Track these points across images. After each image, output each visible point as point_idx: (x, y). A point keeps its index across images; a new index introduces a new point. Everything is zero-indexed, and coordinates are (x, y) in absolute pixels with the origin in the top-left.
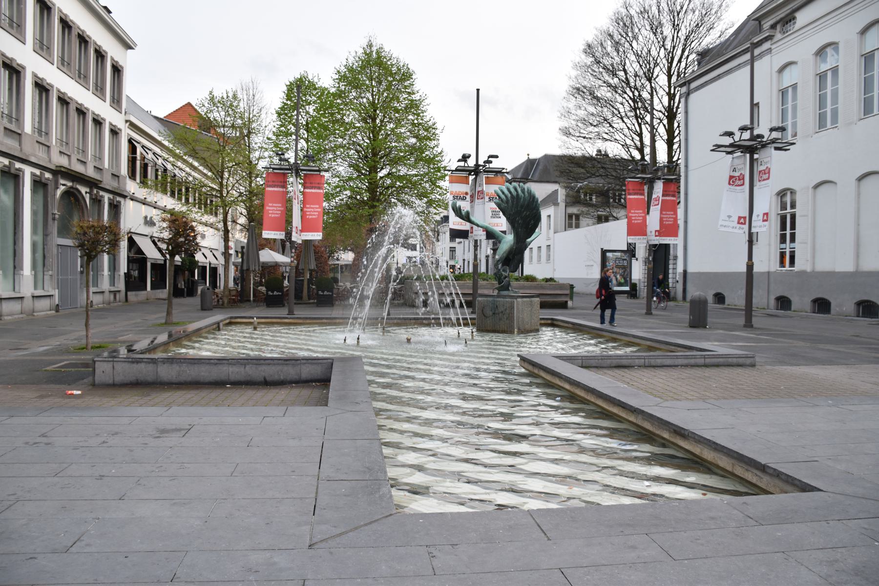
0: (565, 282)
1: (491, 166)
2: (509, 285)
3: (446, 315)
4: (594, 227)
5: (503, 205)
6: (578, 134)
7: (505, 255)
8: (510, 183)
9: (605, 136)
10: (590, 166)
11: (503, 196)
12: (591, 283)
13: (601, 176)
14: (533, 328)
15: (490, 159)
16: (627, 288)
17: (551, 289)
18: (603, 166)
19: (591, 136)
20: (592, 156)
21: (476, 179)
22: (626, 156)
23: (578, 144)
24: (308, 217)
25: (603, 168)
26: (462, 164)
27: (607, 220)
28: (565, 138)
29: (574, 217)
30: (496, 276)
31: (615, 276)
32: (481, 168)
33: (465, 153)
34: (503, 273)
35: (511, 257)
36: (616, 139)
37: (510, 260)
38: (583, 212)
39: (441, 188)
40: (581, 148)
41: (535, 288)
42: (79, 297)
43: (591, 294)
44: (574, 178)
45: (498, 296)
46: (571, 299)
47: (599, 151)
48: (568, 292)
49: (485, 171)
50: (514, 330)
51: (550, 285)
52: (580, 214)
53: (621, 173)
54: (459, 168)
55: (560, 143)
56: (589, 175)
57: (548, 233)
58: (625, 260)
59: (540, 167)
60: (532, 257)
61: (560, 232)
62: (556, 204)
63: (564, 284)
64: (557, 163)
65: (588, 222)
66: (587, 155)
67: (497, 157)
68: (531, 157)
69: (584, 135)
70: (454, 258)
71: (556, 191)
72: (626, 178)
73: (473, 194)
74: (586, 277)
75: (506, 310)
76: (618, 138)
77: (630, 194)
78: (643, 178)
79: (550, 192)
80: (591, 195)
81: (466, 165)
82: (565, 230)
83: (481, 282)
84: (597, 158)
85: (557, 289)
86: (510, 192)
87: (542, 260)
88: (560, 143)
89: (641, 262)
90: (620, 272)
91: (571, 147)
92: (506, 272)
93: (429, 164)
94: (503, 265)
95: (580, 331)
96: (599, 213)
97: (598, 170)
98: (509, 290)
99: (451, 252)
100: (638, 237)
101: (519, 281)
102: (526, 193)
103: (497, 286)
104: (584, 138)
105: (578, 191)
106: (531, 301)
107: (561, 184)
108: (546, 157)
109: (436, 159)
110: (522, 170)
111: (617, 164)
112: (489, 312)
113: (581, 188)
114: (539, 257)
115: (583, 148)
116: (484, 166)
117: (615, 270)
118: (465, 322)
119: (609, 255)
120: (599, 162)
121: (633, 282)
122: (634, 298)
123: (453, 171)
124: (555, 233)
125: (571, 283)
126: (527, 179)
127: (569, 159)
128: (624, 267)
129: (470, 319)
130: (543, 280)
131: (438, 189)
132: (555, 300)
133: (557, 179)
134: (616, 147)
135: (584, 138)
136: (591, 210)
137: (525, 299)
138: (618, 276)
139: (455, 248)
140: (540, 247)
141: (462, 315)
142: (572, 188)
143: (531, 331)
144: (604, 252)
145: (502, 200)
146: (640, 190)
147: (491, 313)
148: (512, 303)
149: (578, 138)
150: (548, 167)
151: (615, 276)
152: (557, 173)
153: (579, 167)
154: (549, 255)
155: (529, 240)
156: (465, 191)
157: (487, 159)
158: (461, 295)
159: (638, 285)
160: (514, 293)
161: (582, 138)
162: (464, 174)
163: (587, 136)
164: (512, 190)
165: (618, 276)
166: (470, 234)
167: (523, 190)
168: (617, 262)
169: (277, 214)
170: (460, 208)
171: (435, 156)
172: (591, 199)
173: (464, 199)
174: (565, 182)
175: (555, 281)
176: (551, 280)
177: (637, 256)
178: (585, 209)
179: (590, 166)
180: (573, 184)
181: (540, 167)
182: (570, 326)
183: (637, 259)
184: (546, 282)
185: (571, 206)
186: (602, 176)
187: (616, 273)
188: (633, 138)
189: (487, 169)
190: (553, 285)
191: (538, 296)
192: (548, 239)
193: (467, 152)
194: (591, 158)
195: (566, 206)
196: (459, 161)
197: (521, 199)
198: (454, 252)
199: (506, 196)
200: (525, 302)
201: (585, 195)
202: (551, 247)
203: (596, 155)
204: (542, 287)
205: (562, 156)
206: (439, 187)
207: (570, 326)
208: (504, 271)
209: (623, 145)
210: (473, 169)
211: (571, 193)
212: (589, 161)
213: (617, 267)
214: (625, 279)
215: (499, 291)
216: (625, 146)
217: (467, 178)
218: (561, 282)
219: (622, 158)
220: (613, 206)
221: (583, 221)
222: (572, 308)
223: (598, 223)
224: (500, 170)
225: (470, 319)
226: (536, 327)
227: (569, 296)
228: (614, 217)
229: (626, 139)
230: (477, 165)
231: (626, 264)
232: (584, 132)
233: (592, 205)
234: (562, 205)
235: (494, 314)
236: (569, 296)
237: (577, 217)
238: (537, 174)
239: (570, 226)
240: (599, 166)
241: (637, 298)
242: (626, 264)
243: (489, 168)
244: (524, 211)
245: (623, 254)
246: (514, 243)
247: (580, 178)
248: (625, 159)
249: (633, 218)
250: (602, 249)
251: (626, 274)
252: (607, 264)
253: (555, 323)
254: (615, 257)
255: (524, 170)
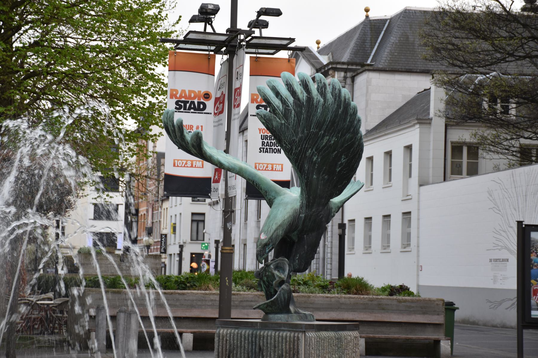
0: (434, 296)
1: (266, 33)
4: (510, 171)
5: (277, 122)
7: (281, 232)
8: (326, 74)
10: (506, 34)
11: (276, 102)
12: (504, 301)
15: (262, 18)
21: (230, 62)
26: (199, 27)
29: (465, 150)
30: (261, 279)
32: (242, 37)
33: (205, 2)
34: (276, 273)
35: (294, 236)
37: (294, 243)
38: (484, 138)
41: (365, 308)
43: (504, 327)
44: (465, 62)
45: (265, 326)
48: (440, 319)
49: (249, 45)
51: (399, 301)
52: (480, 144)
54: (191, 36)
56: (499, 55)
57: (406, 186)
59: (393, 39)
60: (370, 237)
61: (433, 184)
63: (430, 300)
64: (427, 29)
65: (496, 162)
66: (498, 10)
67: (277, 13)
68: (374, 15)
70: (200, 237)
71: (427, 91)
73: (223, 95)
74: (491, 285)
79: (413, 94)
80: (506, 100)
81: (209, 29)
82: (445, 180)
83: (235, 289)
84: (523, 15)
85: (415, 312)
86: (293, 92)
92: (283, 271)
94: (276, 256)
96: (523, 141)
97: (522, 46)
98: (288, 312)
99: (195, 225)
101: (329, 291)
102: (329, 96)
103: (263, 301)
105: (476, 93)
106: (339, 339)
107: (437, 76)
109: (147, 13)
110: (352, 44)
116: (248, 33)
120: (525, 26)
123: (178, 42)
124: (421, 185)
125: (447, 299)
126: (363, 65)
127: (455, 21)
130: (384, 289)
132: (410, 336)
133: (431, 66)
136: (504, 134)
137: (324, 334)
139: (203, 214)
142: (463, 87)
145: (274, 111)
150: (411, 39)
152: (428, 52)
153: (478, 37)
154: (409, 234)
155: (336, 200)
156: (203, 90)
157: (254, 17)
160: (301, 319)
162: (202, 50)
170: (181, 126)
172: (506, 111)
173: (200, 108)
174: (445, 72)
175: (411, 294)
176: (403, 289)
178: (489, 133)
179: (506, 34)
180: (463, 78)
181: (393, 39)
184: (391, 294)
185: (457, 124)
189: (254, 41)
190: (405, 301)
191: (356, 325)
192: (407, 198)
196: (193, 20)
197: (303, 103)
198: (201, 225)
199: (284, 102)
200: (324, 339)
201: (493, 100)
202: (414, 216)
204: (381, 307)
205: (440, 13)
206: (152, 77)
208: (277, 268)
210: (223, 38)
211: (458, 96)
212: (502, 24)
215: (267, 313)
217: (210, 59)
218: (425, 295)
223: (521, 165)
224: (285, 42)
227: (443, 330)
230: (233, 31)
233: (507, 125)
234: (439, 124)
236: (443, 330)
238: (385, 54)
239: (457, 171)
243: (261, 37)
244: (324, 136)
246: (301, 207)
247: (478, 63)
248: (495, 14)
250: (520, 223)
255: (356, 45)
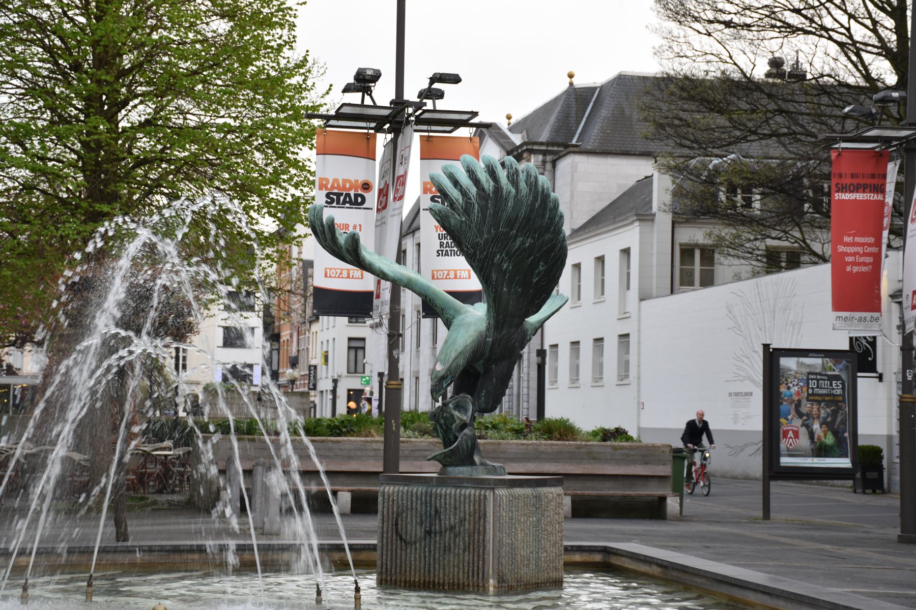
0: (658, 441)
1: (441, 105)
2: (473, 448)
3: (270, 534)
5: (456, 219)
6: (710, 15)
7: (462, 362)
8: (519, 158)
9: (794, 20)
11: (455, 193)
12: (746, 445)
13: (774, 134)
14: (543, 576)
15: (436, 86)
16: (844, 463)
17: (617, 462)
18: (784, 106)
19: (748, 21)
20: (750, 80)
21: (394, 142)
22: (853, 78)
23: (708, 44)
24: (849, 269)
25: (781, 111)
26: (355, 98)
27: (794, 262)
28: (673, 25)
29: (697, 254)
30: (437, 421)
31: (808, 427)
32: (410, 110)
35: (479, 367)
36: (823, 28)
38: (721, 238)
39: (303, 168)
40: (717, 56)
41: (572, 457)
42: (346, 488)
43: (747, 478)
45: (442, 481)
46: (678, 491)
47: (776, 63)
48: (665, 470)
49: (419, 121)
50: (485, 580)
51: (615, 448)
53: (838, 127)
54: (345, 110)
55: (658, 41)
56: (738, 133)
57: (623, 300)
58: (837, 378)
61: (657, 297)
62: (645, 217)
64: (647, 99)
65: (736, 269)
66: (736, 76)
67: (455, 79)
69: (727, 18)
70: (360, 369)
71: (649, 178)
72: (835, 141)
75: (462, 521)
76: (828, 22)
77: (843, 189)
78: (887, 141)
79: (631, 182)
80: (747, 190)
81: (368, 101)
82: (672, 292)
84: (768, 83)
86: (476, 181)
87: (605, 376)
88: (658, 41)
89: (894, 385)
90: (823, 414)
91: (689, 54)
93: (268, 96)
95: (687, 588)
96: (770, 242)
98: (473, 463)
99: (352, 353)
100: (857, 315)
101: (525, 437)
102: (523, 185)
103: (440, 450)
104: (728, 24)
105: (710, 181)
106: (538, 497)
107: (661, 160)
108: (623, 82)
109: (289, 81)
110: (552, 119)
111: (825, 100)
112: (414, 530)
113: (717, 171)
114: (598, 368)
115: (725, 56)
116: (418, 106)
117: (806, 407)
118: (247, 556)
119: (787, 363)
120: (770, 96)
121: (861, 442)
122: (874, 492)
123: (327, 118)
126: (566, 146)
127: (683, 89)
128: (832, 401)
129: (352, 547)
130: (595, 434)
131: (293, 171)
133: (653, 147)
134: (820, 53)
135: (728, 24)
136: (746, 233)
137: (518, 491)
138: (816, 426)
139: (363, 339)
140: (601, 340)
141: (349, 536)
142: (694, 173)
143: (538, 586)
144: (772, 356)
145: (452, 205)
146: (873, 176)
147: (420, 532)
148: (483, 501)
149: (711, 27)
150: (628, 112)
151: (808, 427)
152: (648, 128)
153: (712, 110)
154: (627, 363)
155: (533, 319)
156: (361, 178)
157: (426, 86)
158: (323, 477)
159: (885, 453)
161: (722, 27)
162: (360, 128)
163: (736, 19)
164: (483, 176)
165: (816, 426)
166: (375, 301)
167: (513, 177)
168: (812, 384)
169: (865, 264)
171: (290, 72)
172: (748, 203)
173: (357, 202)
174: (671, 154)
176: (619, 433)
177: (879, 369)
178: (727, 232)
181: (605, 112)
182: (656, 570)
183: (880, 378)
184: (604, 440)
185: (687, 221)
186: (778, 135)
187: (809, 415)
188: (875, 22)
189: (426, 116)
190: (622, 448)
191: (559, 479)
192: (624, 317)
193: (370, 64)
194: (747, 85)
195: (673, 223)
196: (348, 89)
198: (360, 353)
200: (518, 498)
201: (732, 190)
202: (633, 339)
203: (768, 75)
204: (592, 457)
205: (663, 79)
206: (295, 164)
207: (656, 570)
208: (458, 407)
209: (841, 45)
210: (386, 112)
211: (688, 185)
213: (812, 398)
214: (835, 433)
216: (851, 47)
217: (370, 140)
219: (842, 84)
220: (812, 224)
221: (725, 265)
222: (681, 518)
223: (768, 273)
224: (465, 117)
225: (352, 547)
226: (554, 575)
227: (670, 484)
228: (815, 254)
229: (854, 26)
230: (399, 103)
231: (839, 392)
232: (728, 7)
233: (749, 221)
234: (664, 220)
235: (428, 532)
236: (670, 484)
237: (708, 255)
238: (595, 131)
239: (687, 281)
240: (772, 106)
241: (884, 492)
242: (839, 392)
243: (434, 111)
244: (516, 237)
245: (829, 362)
246: (488, 329)
247: (713, 143)
248: (848, 86)
249: (849, 259)
250: (766, 347)
251: (839, 419)
252: (783, 389)
253: (615, 560)
254: (805, 370)
255: (558, 120)
